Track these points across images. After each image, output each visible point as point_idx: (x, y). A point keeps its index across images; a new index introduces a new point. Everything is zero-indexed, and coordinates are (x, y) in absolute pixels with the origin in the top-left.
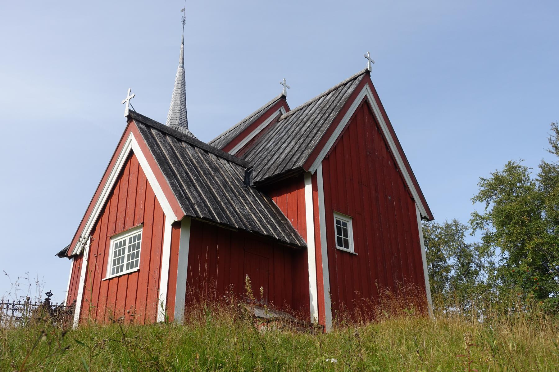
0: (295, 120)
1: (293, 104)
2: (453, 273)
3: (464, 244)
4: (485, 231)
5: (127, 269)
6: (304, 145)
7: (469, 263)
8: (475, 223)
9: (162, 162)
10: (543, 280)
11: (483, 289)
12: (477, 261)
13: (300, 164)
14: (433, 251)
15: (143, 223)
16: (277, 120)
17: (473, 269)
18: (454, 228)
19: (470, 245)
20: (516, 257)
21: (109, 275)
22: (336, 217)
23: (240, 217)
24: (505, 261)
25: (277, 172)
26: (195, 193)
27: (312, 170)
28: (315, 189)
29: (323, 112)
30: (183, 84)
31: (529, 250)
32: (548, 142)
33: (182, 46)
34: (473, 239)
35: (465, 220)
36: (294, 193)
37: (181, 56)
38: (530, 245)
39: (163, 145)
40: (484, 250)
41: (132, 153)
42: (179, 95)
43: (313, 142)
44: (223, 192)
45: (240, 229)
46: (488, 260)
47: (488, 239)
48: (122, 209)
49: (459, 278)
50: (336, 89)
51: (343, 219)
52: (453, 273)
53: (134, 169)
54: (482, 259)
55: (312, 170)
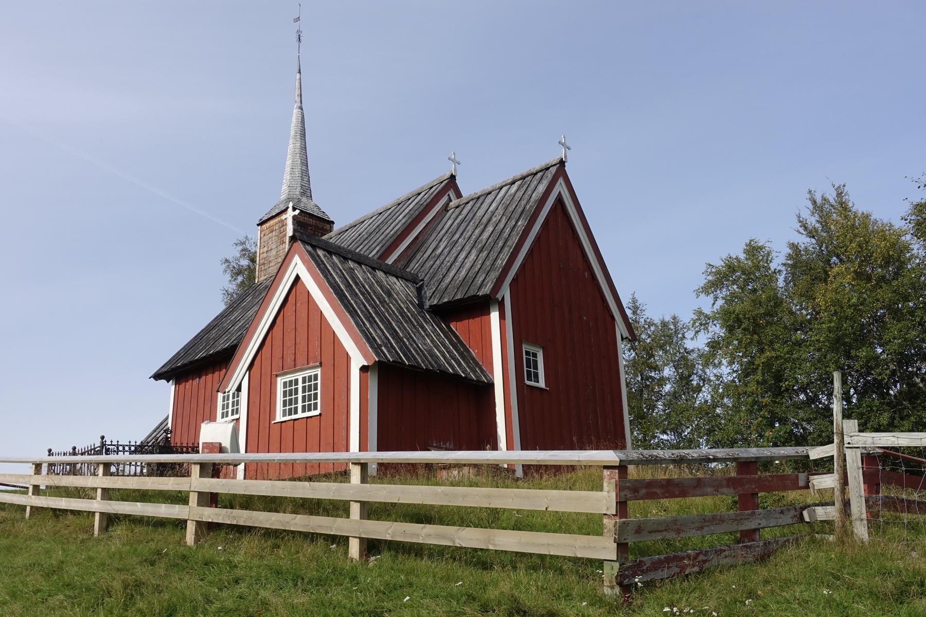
0: (471, 215)
1: (468, 188)
2: (668, 388)
3: (686, 349)
4: (710, 335)
5: (304, 411)
6: (488, 263)
7: (690, 376)
8: (697, 324)
9: (341, 296)
10: (775, 402)
11: (707, 411)
12: (700, 372)
13: (486, 290)
14: (642, 357)
15: (321, 363)
16: (446, 208)
17: (695, 383)
18: (672, 327)
19: (693, 350)
20: (747, 371)
21: (279, 418)
22: (525, 347)
23: (424, 355)
24: (735, 375)
25: (459, 297)
26: (378, 331)
27: (499, 296)
28: (502, 317)
29: (508, 213)
30: (303, 135)
31: (759, 365)
32: (796, 219)
33: (298, 75)
34: (697, 342)
35: (686, 317)
36: (478, 319)
37: (298, 92)
38: (760, 360)
39: (335, 271)
40: (708, 359)
41: (298, 278)
42: (298, 151)
43: (499, 262)
44: (401, 323)
45: (427, 369)
46: (715, 371)
47: (714, 345)
48: (289, 343)
49: (675, 395)
50: (523, 178)
51: (532, 349)
52: (668, 388)
53: (302, 299)
54: (707, 371)
55: (499, 296)
